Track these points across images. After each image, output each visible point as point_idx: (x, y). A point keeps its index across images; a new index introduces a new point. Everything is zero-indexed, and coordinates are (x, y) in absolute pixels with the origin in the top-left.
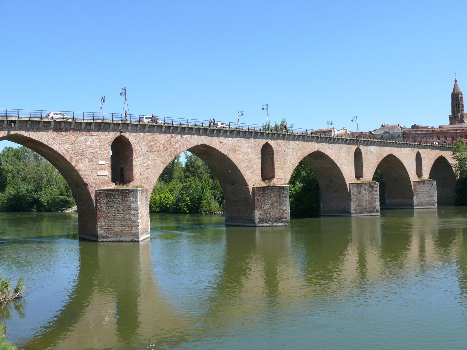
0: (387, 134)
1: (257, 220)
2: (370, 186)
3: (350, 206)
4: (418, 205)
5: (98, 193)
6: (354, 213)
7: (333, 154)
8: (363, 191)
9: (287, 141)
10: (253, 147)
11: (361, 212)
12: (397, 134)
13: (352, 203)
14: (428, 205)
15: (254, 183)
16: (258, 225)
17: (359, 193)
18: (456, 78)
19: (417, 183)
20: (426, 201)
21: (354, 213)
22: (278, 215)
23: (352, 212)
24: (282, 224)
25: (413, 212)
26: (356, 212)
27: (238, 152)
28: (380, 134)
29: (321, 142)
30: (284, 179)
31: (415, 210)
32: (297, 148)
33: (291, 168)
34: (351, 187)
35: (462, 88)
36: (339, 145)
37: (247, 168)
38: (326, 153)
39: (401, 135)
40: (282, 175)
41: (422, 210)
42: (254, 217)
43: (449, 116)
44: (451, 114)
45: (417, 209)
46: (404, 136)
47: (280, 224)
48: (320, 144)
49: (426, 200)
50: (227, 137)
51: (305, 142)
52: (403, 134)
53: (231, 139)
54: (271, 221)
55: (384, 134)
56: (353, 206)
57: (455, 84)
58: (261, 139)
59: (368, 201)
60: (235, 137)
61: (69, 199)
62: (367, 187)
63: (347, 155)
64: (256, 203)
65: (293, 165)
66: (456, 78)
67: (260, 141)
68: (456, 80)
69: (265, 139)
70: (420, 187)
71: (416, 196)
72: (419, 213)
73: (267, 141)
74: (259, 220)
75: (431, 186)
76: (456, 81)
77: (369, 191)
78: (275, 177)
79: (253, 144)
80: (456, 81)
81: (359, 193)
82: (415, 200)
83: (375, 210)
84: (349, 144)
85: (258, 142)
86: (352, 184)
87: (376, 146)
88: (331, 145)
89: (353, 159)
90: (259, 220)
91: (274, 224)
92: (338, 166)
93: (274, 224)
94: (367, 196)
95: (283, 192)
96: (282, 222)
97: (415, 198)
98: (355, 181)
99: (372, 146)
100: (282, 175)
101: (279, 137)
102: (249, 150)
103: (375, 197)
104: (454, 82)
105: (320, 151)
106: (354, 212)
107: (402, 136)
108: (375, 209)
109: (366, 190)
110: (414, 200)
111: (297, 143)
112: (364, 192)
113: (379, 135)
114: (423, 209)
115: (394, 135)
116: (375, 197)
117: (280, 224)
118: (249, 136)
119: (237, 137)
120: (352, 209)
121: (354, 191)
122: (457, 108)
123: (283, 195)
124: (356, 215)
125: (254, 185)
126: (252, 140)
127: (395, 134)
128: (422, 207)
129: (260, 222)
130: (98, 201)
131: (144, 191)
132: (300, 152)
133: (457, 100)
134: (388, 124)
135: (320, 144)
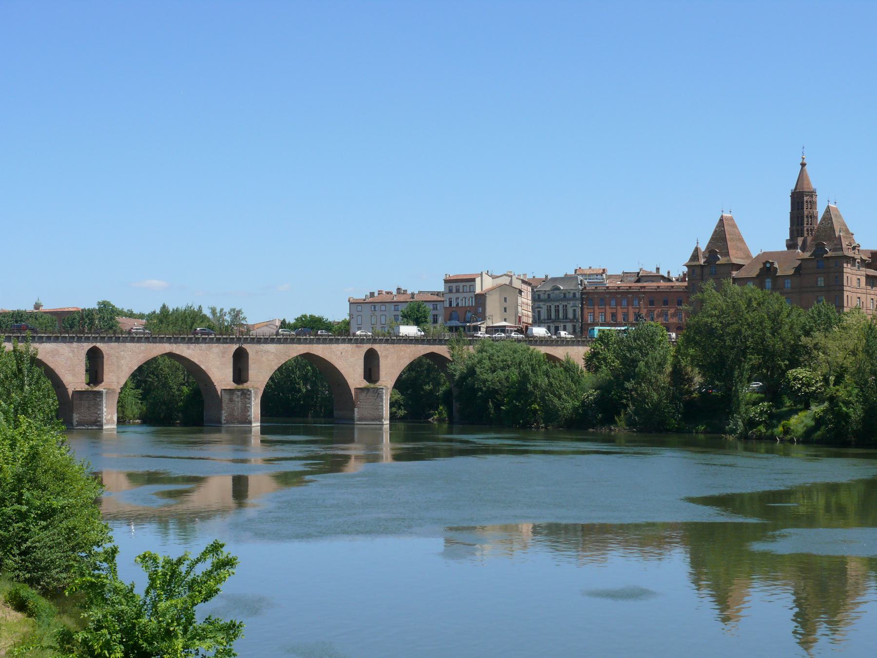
0: (557, 292)
1: (75, 423)
2: (242, 394)
3: (221, 414)
4: (360, 419)
5: (76, 393)
6: (225, 424)
7: (196, 355)
8: (235, 397)
9: (123, 344)
10: (76, 351)
11: (232, 423)
12: (572, 292)
13: (223, 412)
14: (373, 420)
15: (75, 387)
16: (75, 428)
17: (231, 400)
18: (803, 159)
19: (359, 391)
20: (369, 415)
21: (225, 424)
22: (93, 418)
23: (223, 422)
24: (96, 427)
25: (353, 429)
26: (227, 423)
27: (56, 356)
28: (545, 291)
29: (176, 343)
30: (116, 384)
31: (356, 426)
32: (137, 351)
33: (128, 372)
34: (223, 394)
35: (815, 182)
36: (207, 345)
37: (67, 372)
38: (183, 355)
39: (578, 295)
40: (114, 379)
41: (365, 426)
42: (72, 420)
43: (787, 240)
44: (789, 238)
45: (357, 424)
46: (583, 296)
47: (94, 428)
48: (174, 344)
49: (370, 414)
50: (43, 342)
51: (151, 343)
52: (582, 294)
53: (48, 344)
54: (87, 425)
55: (552, 291)
56: (224, 415)
57: (802, 172)
58: (86, 342)
59: (240, 411)
60: (54, 342)
61: (70, 563)
62: (239, 393)
63: (221, 356)
64: (74, 406)
65: (130, 368)
66: (803, 159)
67: (85, 344)
68: (805, 161)
69: (92, 343)
70: (363, 396)
71: (358, 408)
72: (360, 429)
73: (94, 344)
74: (76, 423)
75: (377, 394)
76: (803, 165)
77: (241, 399)
78: (104, 381)
79: (76, 348)
80: (803, 165)
81: (231, 400)
82: (357, 412)
83: (247, 421)
84: (224, 343)
85: (83, 346)
86: (224, 389)
87: (276, 343)
88: (192, 346)
89: (232, 360)
90: (76, 423)
91: (90, 427)
92: (203, 369)
93: (90, 427)
94: (240, 404)
95: (98, 396)
96: (97, 426)
97: (356, 409)
98: (232, 385)
99: (268, 343)
100: (114, 379)
101: (112, 340)
102: (71, 355)
103: (247, 405)
104: (800, 166)
105: (174, 352)
106: (225, 422)
107: (580, 296)
108: (247, 419)
109: (238, 397)
110: (355, 412)
111: (138, 345)
112: (236, 400)
113: (544, 292)
114: (365, 424)
115: (567, 295)
116: (247, 405)
117: (94, 428)
118: (71, 341)
119: (55, 342)
120: (223, 418)
121: (226, 398)
122: (798, 224)
123: (98, 399)
124: (227, 425)
125: (75, 389)
126: (75, 345)
127: (569, 293)
128: (365, 423)
129: (77, 425)
130: (840, 602)
131: (387, 388)
132: (142, 355)
133: (800, 207)
134: (590, 268)
135: (175, 345)
